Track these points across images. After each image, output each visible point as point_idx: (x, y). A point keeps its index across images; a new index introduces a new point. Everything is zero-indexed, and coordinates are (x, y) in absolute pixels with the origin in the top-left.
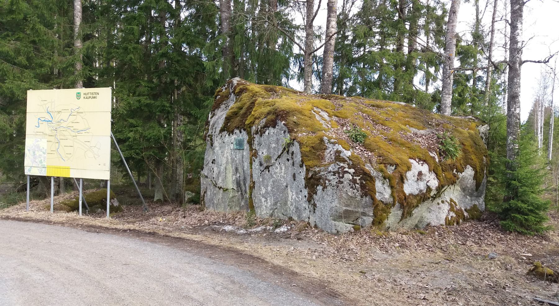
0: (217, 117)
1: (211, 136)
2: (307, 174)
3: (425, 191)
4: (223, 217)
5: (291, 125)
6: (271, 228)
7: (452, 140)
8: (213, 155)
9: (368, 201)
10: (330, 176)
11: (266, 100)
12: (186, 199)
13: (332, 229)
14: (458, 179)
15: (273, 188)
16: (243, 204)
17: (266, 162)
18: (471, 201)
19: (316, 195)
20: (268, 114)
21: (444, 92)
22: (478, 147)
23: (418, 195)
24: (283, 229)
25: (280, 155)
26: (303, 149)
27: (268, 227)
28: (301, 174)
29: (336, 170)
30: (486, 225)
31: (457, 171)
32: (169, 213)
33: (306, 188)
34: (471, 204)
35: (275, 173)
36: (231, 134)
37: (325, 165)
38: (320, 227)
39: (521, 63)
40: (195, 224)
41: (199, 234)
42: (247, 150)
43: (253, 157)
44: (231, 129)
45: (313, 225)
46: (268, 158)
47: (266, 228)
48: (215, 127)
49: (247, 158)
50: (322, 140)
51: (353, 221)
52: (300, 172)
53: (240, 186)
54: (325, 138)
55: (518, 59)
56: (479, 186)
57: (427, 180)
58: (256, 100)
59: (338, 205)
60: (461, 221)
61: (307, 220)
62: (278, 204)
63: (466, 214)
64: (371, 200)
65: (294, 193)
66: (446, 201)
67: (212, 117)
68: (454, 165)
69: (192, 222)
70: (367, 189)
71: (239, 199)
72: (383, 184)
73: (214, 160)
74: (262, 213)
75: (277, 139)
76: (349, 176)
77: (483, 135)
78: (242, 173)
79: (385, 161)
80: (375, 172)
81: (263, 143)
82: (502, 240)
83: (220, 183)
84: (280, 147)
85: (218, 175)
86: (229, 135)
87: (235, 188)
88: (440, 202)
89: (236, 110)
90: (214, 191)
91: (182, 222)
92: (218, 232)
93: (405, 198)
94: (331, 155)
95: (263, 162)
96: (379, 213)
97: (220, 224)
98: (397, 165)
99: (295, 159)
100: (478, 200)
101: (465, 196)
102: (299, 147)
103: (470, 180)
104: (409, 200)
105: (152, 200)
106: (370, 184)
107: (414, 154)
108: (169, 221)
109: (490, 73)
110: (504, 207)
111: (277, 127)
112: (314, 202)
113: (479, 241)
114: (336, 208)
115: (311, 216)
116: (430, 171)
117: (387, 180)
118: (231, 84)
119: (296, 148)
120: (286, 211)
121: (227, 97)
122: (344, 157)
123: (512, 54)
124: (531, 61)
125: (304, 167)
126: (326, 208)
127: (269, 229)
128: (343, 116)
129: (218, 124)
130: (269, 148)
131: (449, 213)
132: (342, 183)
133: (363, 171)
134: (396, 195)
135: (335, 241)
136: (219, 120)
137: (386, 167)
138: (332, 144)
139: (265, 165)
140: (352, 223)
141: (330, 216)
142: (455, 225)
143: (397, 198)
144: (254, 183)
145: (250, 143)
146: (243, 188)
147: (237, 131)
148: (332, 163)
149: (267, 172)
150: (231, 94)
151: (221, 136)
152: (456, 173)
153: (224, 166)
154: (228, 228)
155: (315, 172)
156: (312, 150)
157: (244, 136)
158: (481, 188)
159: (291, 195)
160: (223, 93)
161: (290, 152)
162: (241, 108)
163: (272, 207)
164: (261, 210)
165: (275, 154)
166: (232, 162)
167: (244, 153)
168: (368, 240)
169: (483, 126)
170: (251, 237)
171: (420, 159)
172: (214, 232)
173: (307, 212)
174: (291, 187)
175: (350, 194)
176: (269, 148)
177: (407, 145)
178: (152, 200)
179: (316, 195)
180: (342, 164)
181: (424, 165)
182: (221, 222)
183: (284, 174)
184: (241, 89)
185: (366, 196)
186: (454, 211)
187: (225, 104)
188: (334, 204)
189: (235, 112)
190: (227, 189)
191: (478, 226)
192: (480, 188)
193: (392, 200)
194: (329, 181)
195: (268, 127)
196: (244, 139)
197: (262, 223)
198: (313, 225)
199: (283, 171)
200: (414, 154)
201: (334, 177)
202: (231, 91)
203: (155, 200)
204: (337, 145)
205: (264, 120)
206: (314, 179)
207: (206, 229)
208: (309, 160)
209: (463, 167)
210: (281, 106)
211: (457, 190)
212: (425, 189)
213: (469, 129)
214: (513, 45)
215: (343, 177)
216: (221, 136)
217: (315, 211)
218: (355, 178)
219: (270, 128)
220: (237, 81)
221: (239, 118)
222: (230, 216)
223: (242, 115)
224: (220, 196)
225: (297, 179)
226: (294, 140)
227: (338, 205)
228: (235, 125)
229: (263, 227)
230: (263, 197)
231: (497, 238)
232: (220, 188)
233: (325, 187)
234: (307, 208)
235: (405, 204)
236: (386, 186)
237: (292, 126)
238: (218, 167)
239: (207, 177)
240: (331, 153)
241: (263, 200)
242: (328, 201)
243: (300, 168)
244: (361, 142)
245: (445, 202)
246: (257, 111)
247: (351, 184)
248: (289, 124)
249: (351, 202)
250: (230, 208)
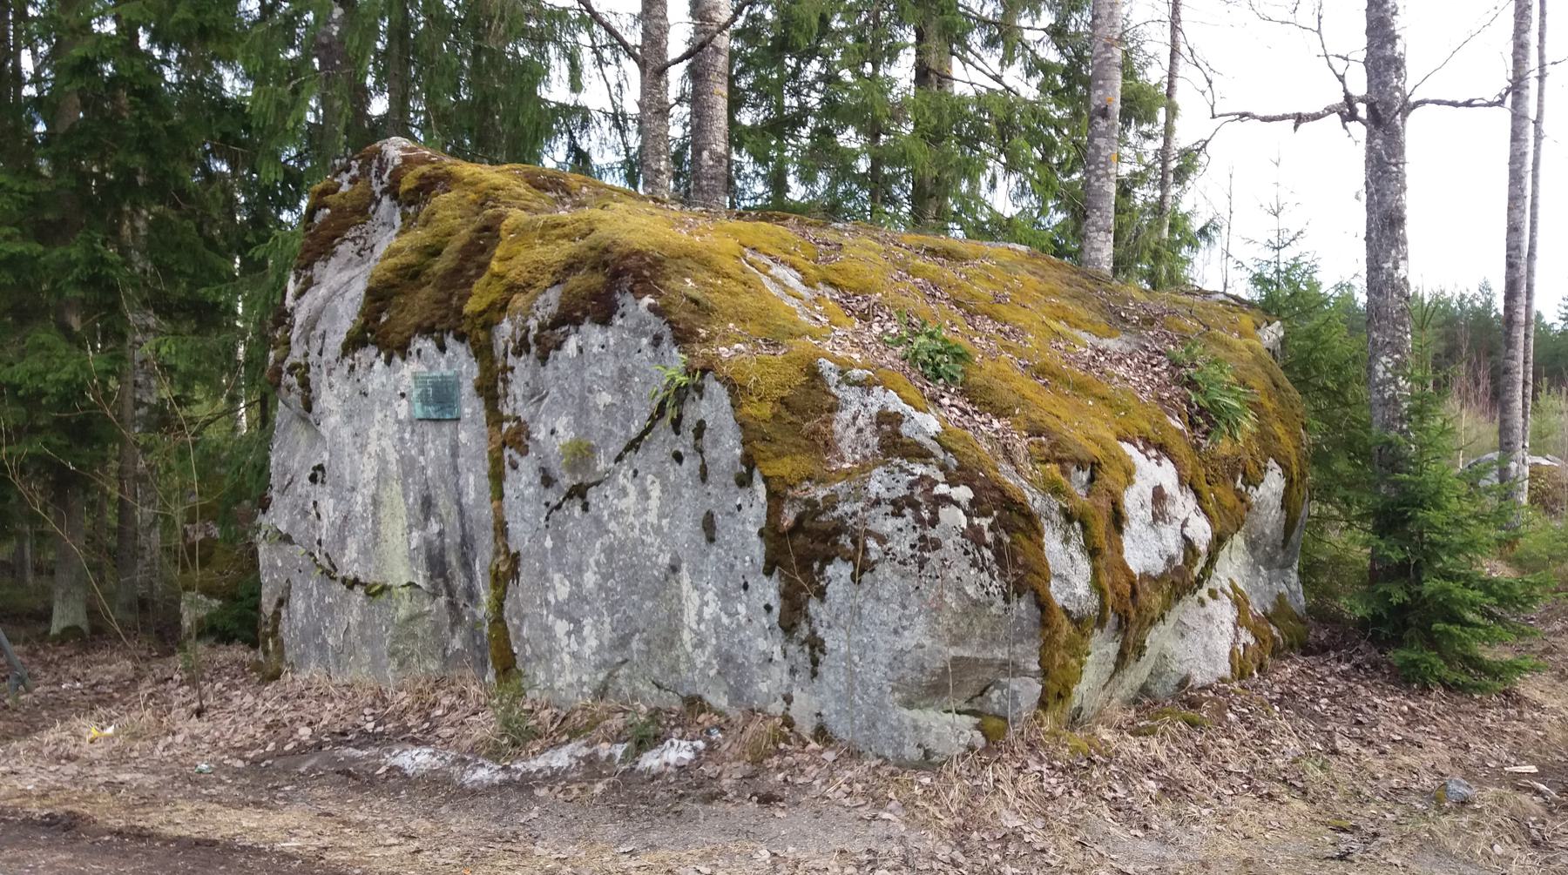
0: (323, 291)
1: (302, 372)
2: (774, 511)
4: (373, 705)
5: (681, 313)
6: (619, 750)
8: (311, 446)
9: (1024, 615)
10: (880, 519)
11: (544, 216)
12: (186, 623)
13: (901, 745)
15: (606, 577)
16: (457, 643)
17: (573, 468)
19: (823, 601)
20: (571, 267)
21: (1094, 224)
24: (676, 752)
25: (641, 437)
26: (747, 409)
27: (604, 749)
28: (740, 515)
29: (901, 491)
31: (1247, 483)
32: (127, 686)
33: (768, 572)
34: (1271, 592)
35: (616, 514)
36: (397, 360)
37: (848, 474)
38: (843, 735)
39: (1407, 108)
40: (253, 746)
41: (288, 799)
42: (473, 421)
43: (507, 452)
44: (399, 338)
45: (807, 728)
46: (581, 455)
47: (595, 754)
48: (318, 332)
49: (475, 457)
50: (814, 374)
51: (970, 701)
52: (739, 507)
53: (442, 574)
54: (825, 365)
55: (1397, 94)
56: (1293, 531)
58: (500, 218)
59: (927, 642)
61: (777, 707)
62: (635, 645)
64: (1034, 608)
65: (710, 596)
66: (1223, 591)
67: (299, 295)
69: (238, 737)
71: (437, 628)
73: (320, 468)
74: (557, 685)
75: (623, 370)
76: (957, 518)
78: (454, 519)
79: (1058, 454)
80: (1039, 498)
81: (554, 390)
83: (350, 562)
84: (636, 406)
85: (341, 529)
86: (388, 362)
87: (421, 582)
89: (412, 258)
90: (321, 598)
91: (193, 737)
92: (371, 784)
93: (1134, 593)
94: (860, 431)
95: (557, 469)
96: (1058, 660)
97: (366, 739)
99: (711, 454)
100: (1286, 578)
102: (727, 402)
105: (41, 629)
106: (1025, 543)
107: (1124, 421)
108: (135, 736)
109: (1171, 176)
111: (618, 321)
112: (814, 633)
114: (920, 652)
115: (796, 693)
116: (1181, 482)
117: (1077, 525)
118: (375, 163)
119: (713, 407)
120: (674, 669)
121: (361, 210)
122: (920, 438)
123: (1378, 75)
124: (1438, 102)
125: (760, 489)
126: (869, 654)
127: (611, 757)
128: (853, 284)
129: (334, 319)
130: (582, 410)
132: (937, 545)
133: (1002, 492)
134: (1105, 580)
135: (932, 795)
136: (337, 301)
137: (1065, 472)
138: (858, 389)
139: (567, 481)
140: (967, 707)
141: (894, 689)
143: (1110, 597)
144: (515, 559)
145: (490, 391)
146: (460, 581)
147: (427, 345)
148: (875, 466)
149: (577, 511)
150: (378, 202)
151: (352, 368)
153: (368, 491)
154: (415, 759)
155: (811, 503)
156: (785, 413)
157: (460, 364)
159: (697, 602)
160: (344, 196)
161: (689, 422)
162: (434, 252)
163: (607, 656)
164: (548, 670)
165: (610, 433)
166: (406, 475)
167: (463, 437)
168: (1054, 781)
169: (1269, 325)
170: (532, 797)
172: (352, 783)
173: (779, 674)
174: (696, 573)
175: (970, 590)
176: (582, 410)
178: (41, 629)
179: (823, 601)
180: (919, 469)
182: (370, 726)
183: (661, 516)
184: (423, 176)
187: (353, 240)
188: (908, 640)
189: (409, 266)
190: (385, 588)
193: (1096, 602)
194: (882, 540)
195: (577, 323)
196: (459, 374)
197: (568, 728)
198: (807, 728)
199: (654, 503)
200: (1124, 421)
201: (900, 522)
202: (377, 189)
203: (55, 629)
204: (877, 390)
205: (554, 295)
206: (808, 533)
207: (312, 769)
208: (778, 455)
210: (624, 237)
211: (1238, 548)
212: (1182, 553)
214: (1381, 47)
215: (934, 522)
216: (352, 368)
217: (820, 669)
219: (586, 327)
220: (403, 149)
221: (428, 290)
222: (405, 699)
223: (444, 277)
224: (354, 617)
225: (722, 535)
226: (704, 371)
227: (927, 642)
228: (416, 319)
229: (579, 748)
230: (560, 613)
232: (352, 584)
233: (863, 568)
234: (778, 656)
236: (1074, 549)
237: (684, 314)
238: (340, 499)
239: (287, 539)
240: (861, 422)
241: (561, 627)
242: (883, 623)
243: (735, 488)
244: (953, 378)
245: (1220, 593)
246: (510, 261)
247: (970, 549)
248: (673, 309)
249: (971, 624)
250: (401, 664)
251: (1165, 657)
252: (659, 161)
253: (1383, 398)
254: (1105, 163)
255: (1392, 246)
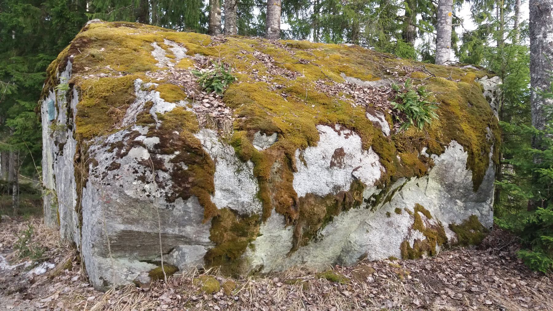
3: (347, 189)
7: (420, 94)
14: (431, 167)
18: (466, 208)
22: (475, 109)
23: (329, 196)
30: (490, 258)
31: (429, 152)
57: (355, 166)
60: (438, 248)
63: (449, 235)
66: (406, 209)
68: (421, 140)
70: (189, 183)
72: (239, 171)
77: (491, 95)
82: (520, 293)
88: (392, 211)
98: (280, 133)
100: (481, 208)
101: (452, 199)
103: (459, 170)
104: (306, 206)
110: (525, 221)
113: (467, 295)
116: (364, 148)
117: (250, 163)
131: (410, 233)
133: (184, 141)
134: (271, 196)
142: (424, 257)
152: (427, 156)
158: (483, 185)
171: (344, 126)
177: (320, 101)
181: (351, 137)
185: (185, 198)
186: (421, 230)
191: (473, 260)
192: (481, 186)
209: (441, 145)
212: (349, 185)
213: (461, 80)
218: (159, 156)
231: (511, 289)
235: (295, 216)
244: (219, 90)
245: (403, 211)
251: (350, 242)
252: (230, 28)
253: (536, 109)
254: (445, 17)
255: (542, 25)
